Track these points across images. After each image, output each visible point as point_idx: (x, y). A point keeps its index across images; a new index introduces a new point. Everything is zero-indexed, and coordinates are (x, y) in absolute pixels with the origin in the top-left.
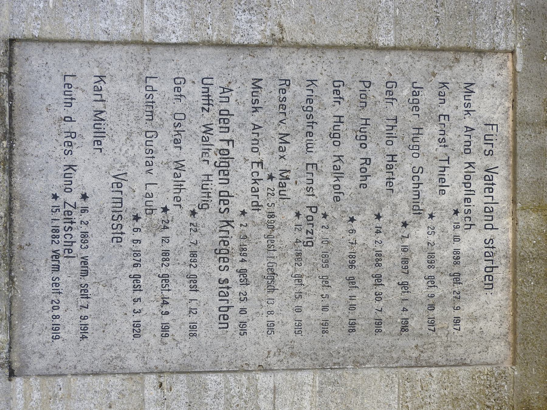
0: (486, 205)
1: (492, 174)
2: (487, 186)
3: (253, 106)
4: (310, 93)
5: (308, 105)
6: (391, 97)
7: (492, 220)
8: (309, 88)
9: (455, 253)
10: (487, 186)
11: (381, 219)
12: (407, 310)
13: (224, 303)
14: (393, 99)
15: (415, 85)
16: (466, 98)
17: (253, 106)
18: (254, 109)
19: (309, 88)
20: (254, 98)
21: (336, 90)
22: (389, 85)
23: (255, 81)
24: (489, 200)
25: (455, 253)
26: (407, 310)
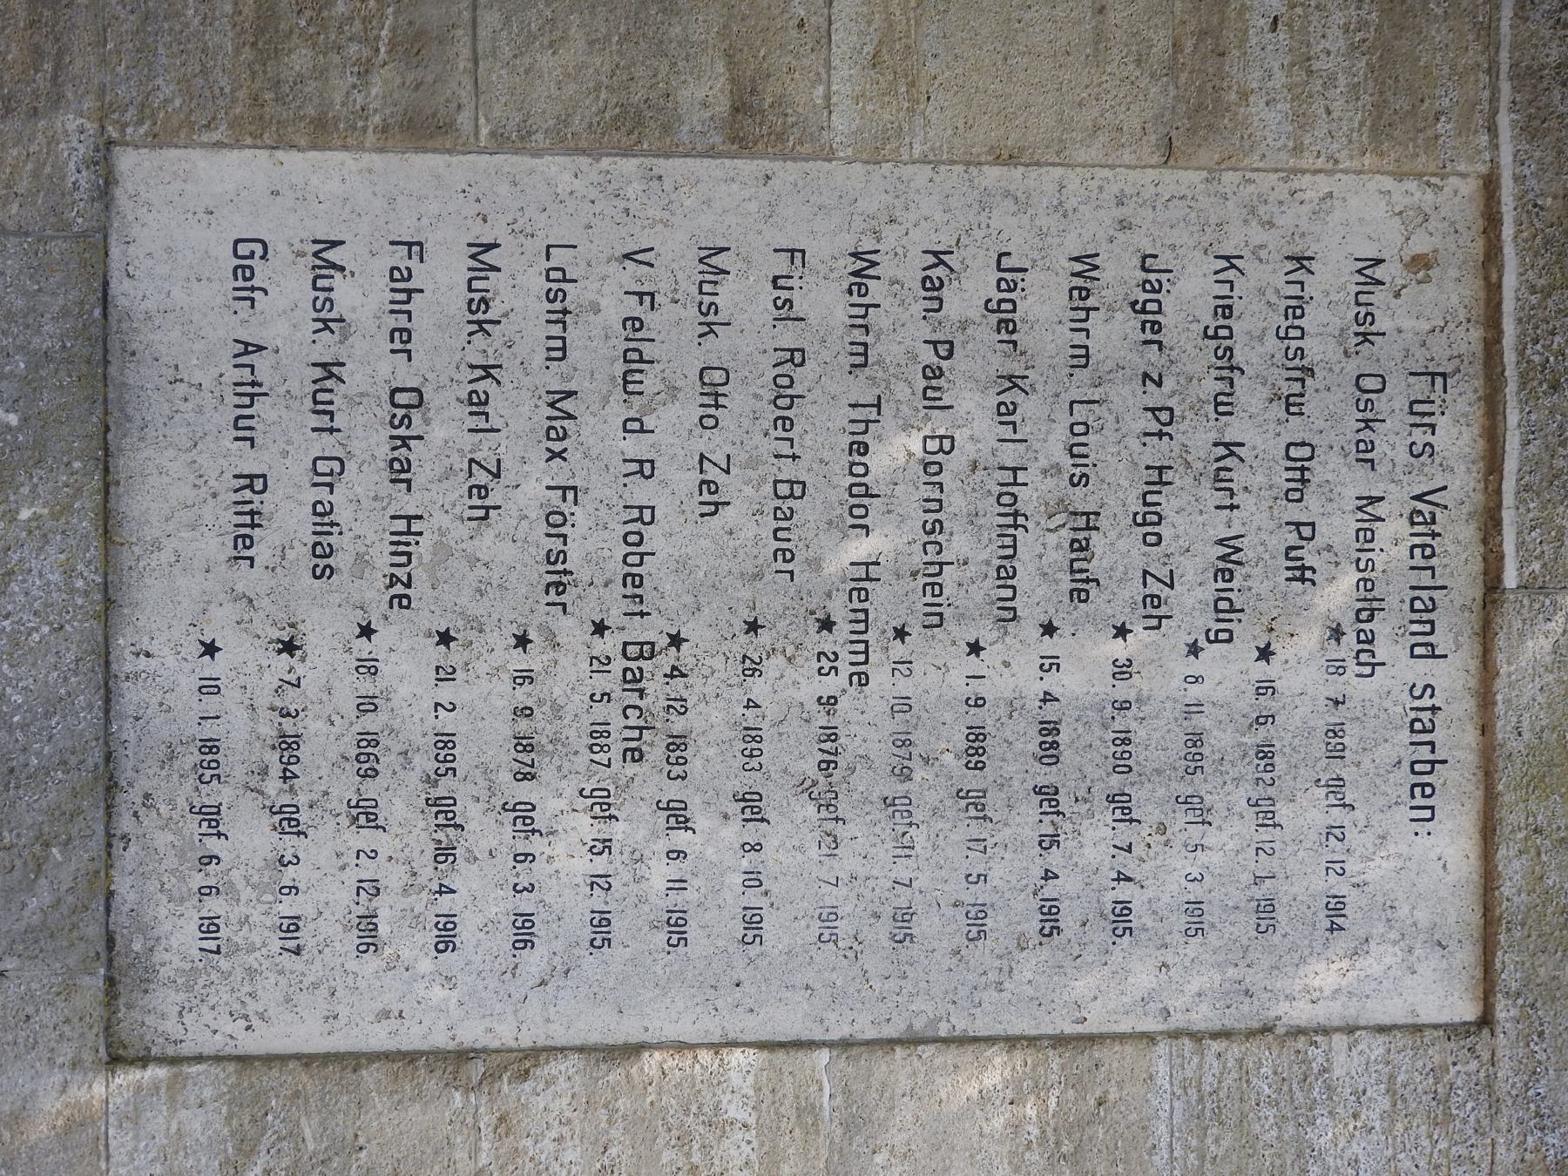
0: (1417, 593)
1: (1431, 508)
2: (1417, 540)
3: (703, 319)
4: (1224, 290)
5: (1222, 322)
6: (249, 284)
7: (1432, 632)
8: (1221, 277)
9: (971, 751)
10: (1417, 540)
11: (685, 646)
12: (1057, 877)
13: (1424, 753)
14: (253, 289)
15: (1005, 262)
16: (706, 288)
17: (703, 319)
18: (320, 325)
19: (1221, 277)
20: (707, 299)
21: (243, 267)
22: (243, 249)
23: (707, 252)
24: (1425, 578)
25: (971, 751)
26: (1057, 877)
